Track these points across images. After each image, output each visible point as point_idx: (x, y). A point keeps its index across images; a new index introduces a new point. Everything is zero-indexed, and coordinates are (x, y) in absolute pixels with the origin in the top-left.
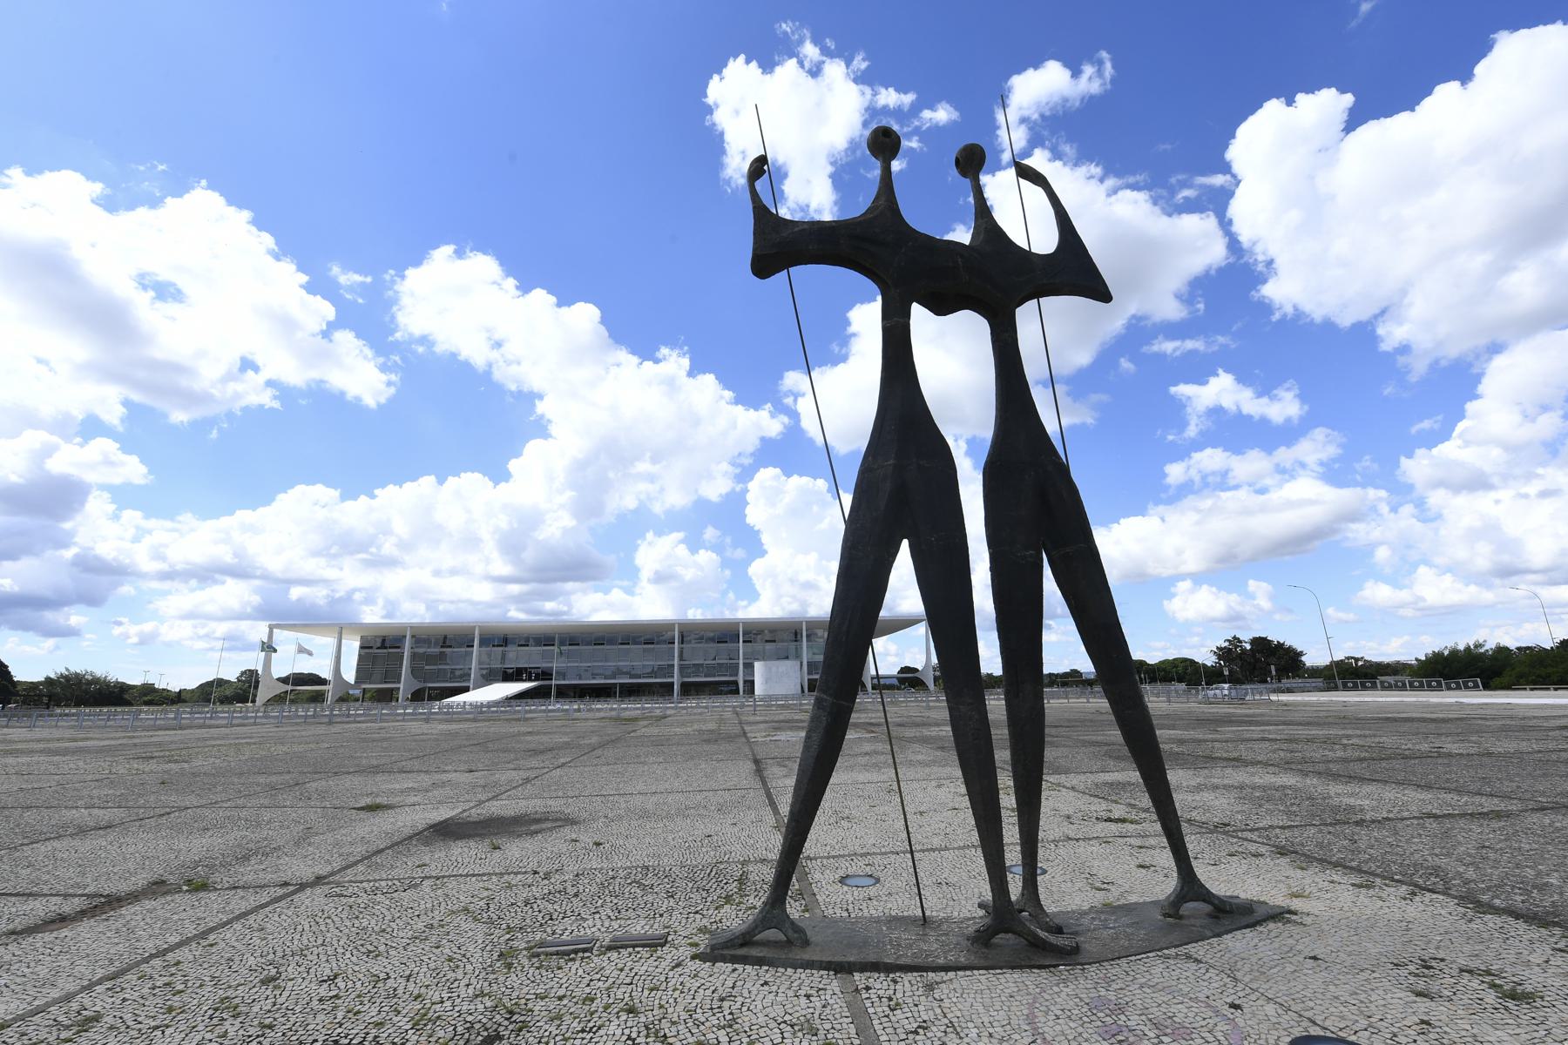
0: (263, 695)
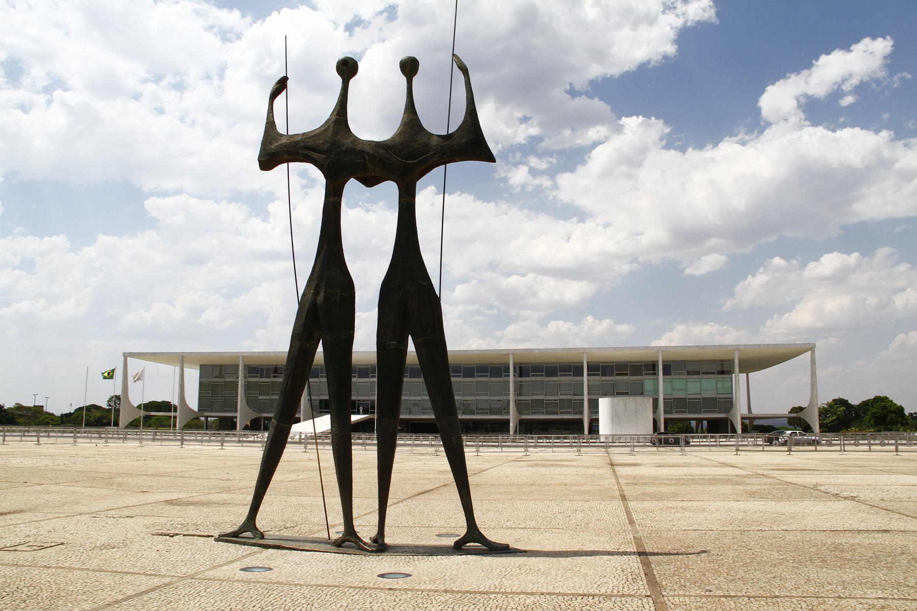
0: (124, 420)
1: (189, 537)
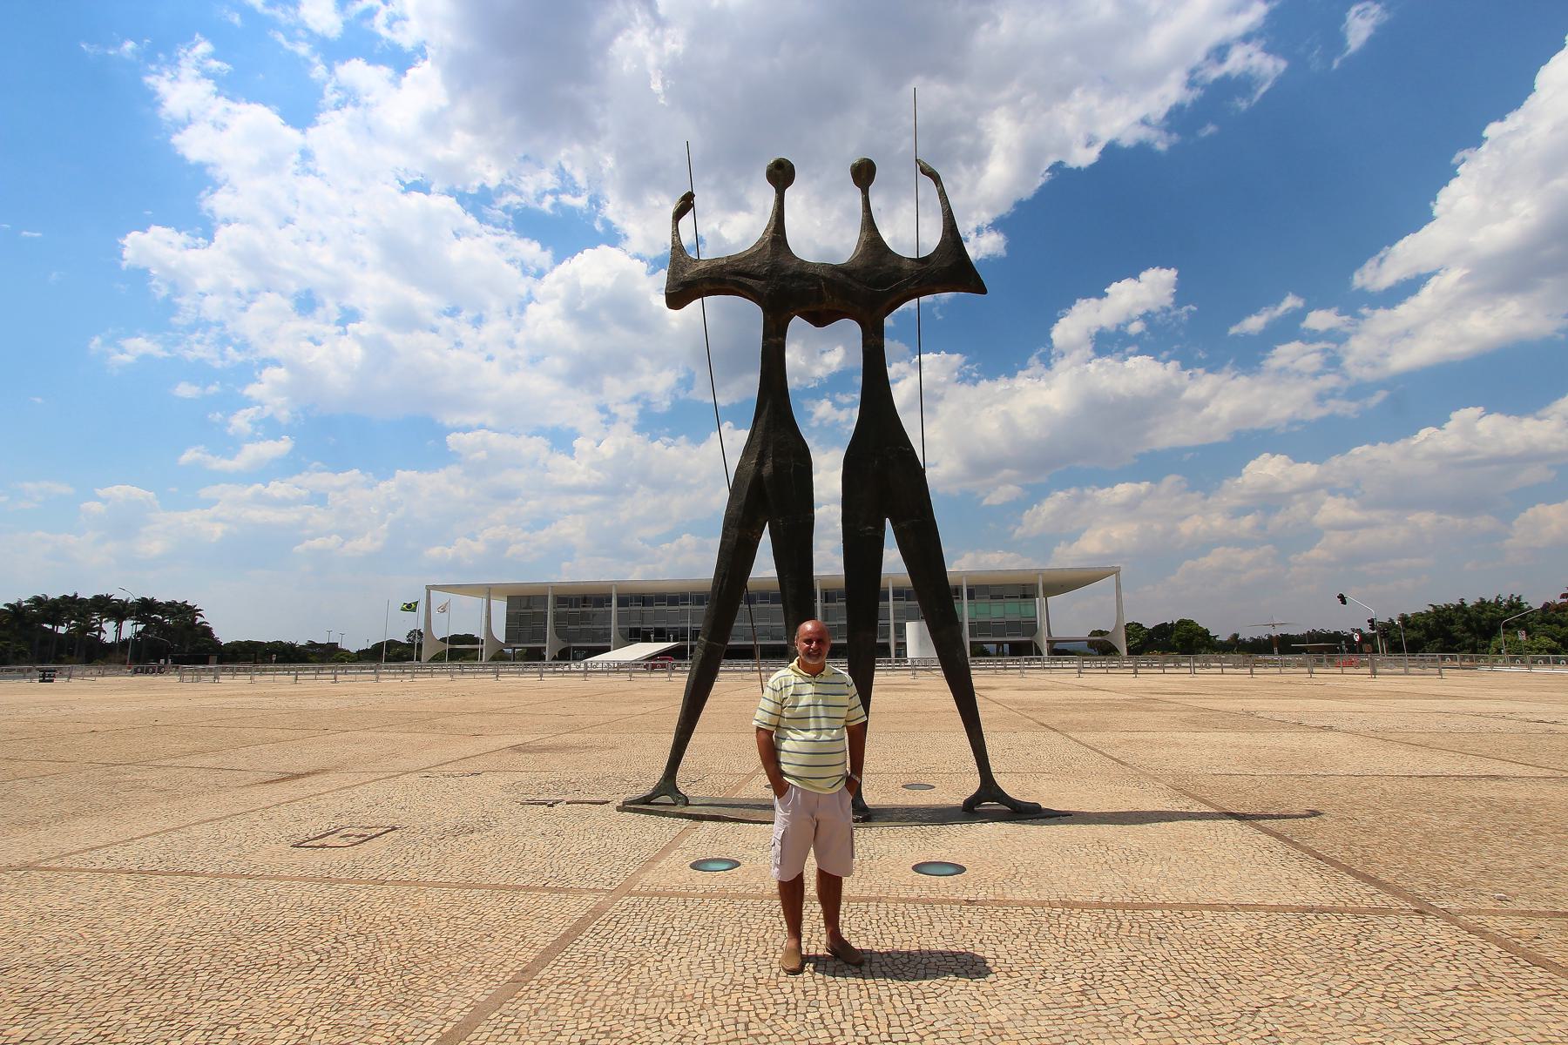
0: (426, 654)
1: (576, 805)
